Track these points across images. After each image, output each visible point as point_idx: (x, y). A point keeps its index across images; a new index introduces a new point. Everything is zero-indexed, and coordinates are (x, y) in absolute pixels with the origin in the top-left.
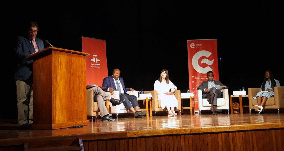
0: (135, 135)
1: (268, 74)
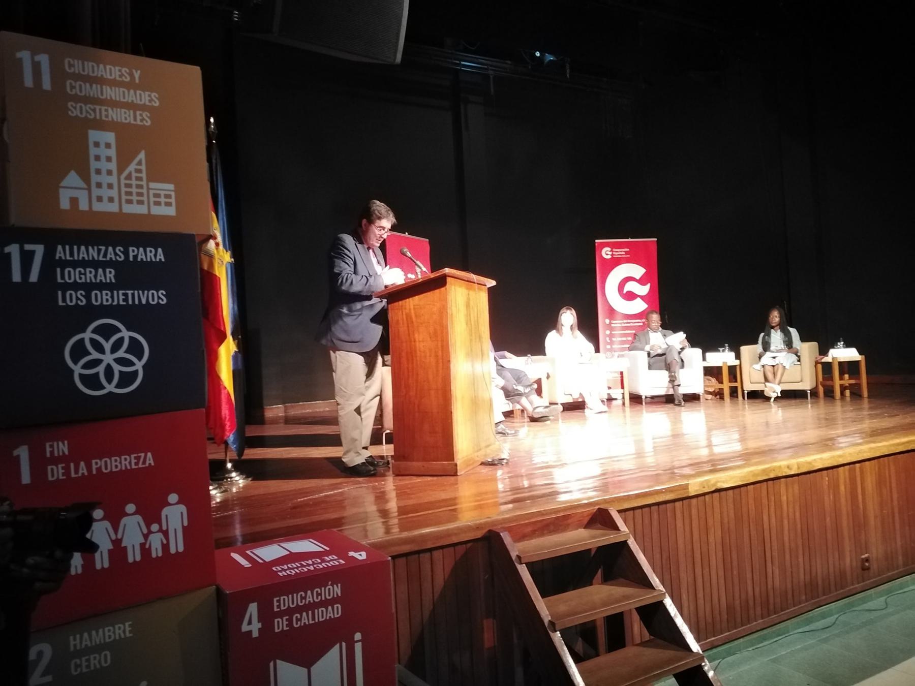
0: (704, 487)
1: (775, 317)
